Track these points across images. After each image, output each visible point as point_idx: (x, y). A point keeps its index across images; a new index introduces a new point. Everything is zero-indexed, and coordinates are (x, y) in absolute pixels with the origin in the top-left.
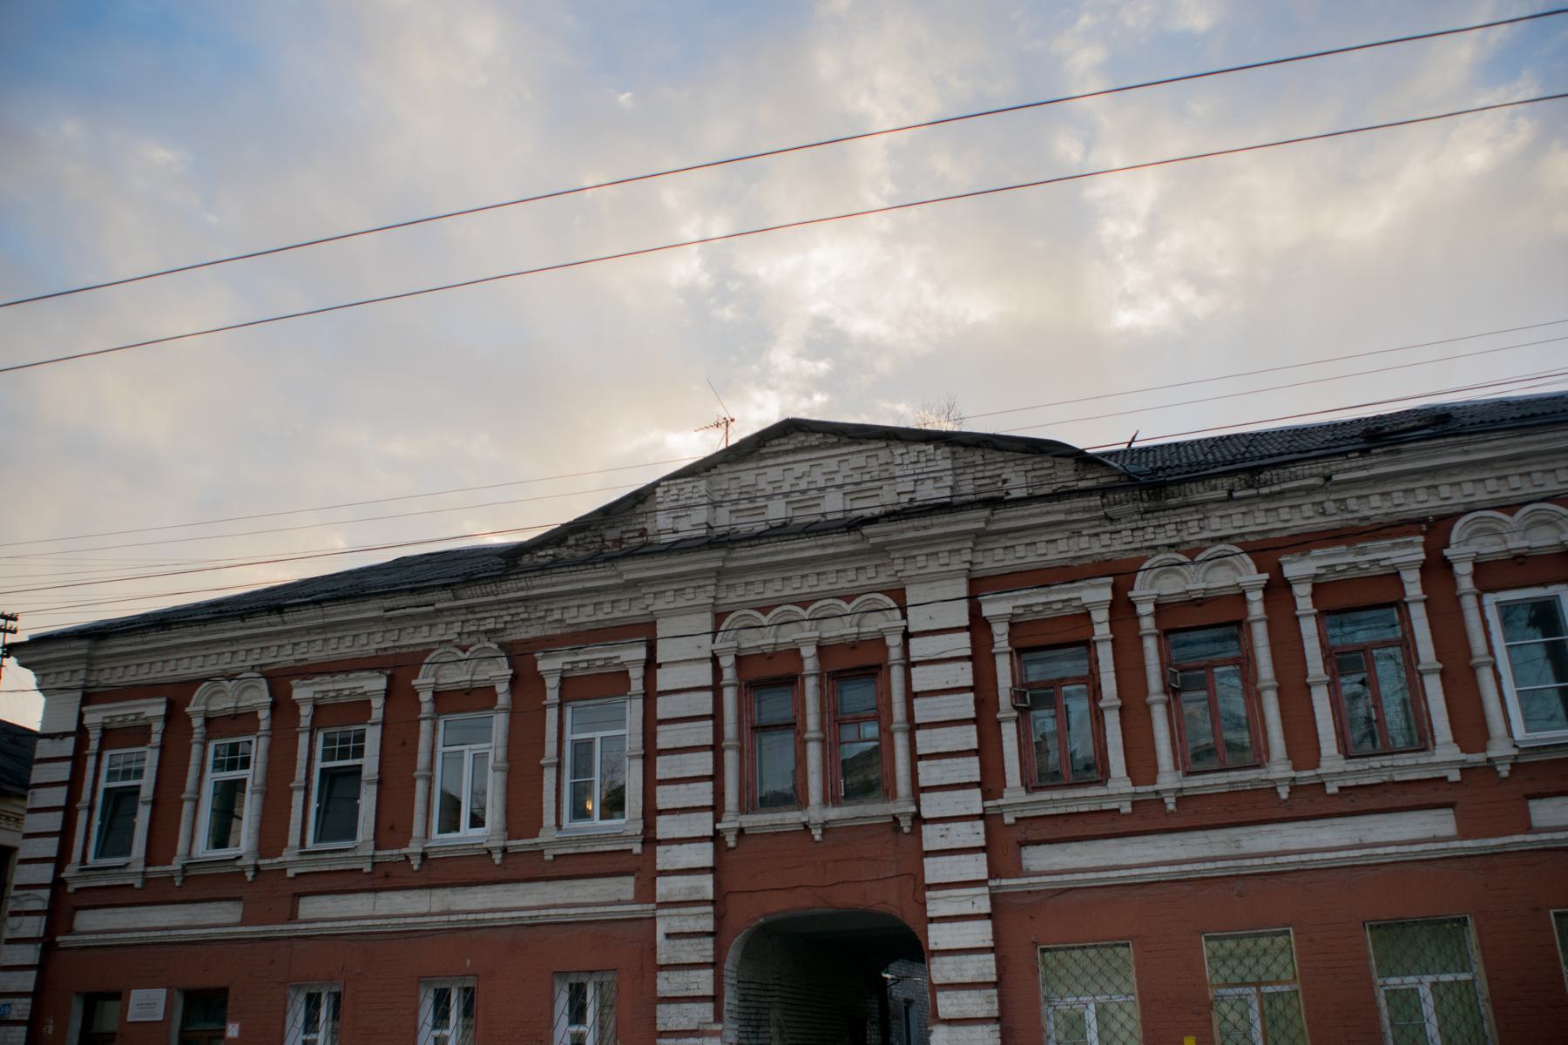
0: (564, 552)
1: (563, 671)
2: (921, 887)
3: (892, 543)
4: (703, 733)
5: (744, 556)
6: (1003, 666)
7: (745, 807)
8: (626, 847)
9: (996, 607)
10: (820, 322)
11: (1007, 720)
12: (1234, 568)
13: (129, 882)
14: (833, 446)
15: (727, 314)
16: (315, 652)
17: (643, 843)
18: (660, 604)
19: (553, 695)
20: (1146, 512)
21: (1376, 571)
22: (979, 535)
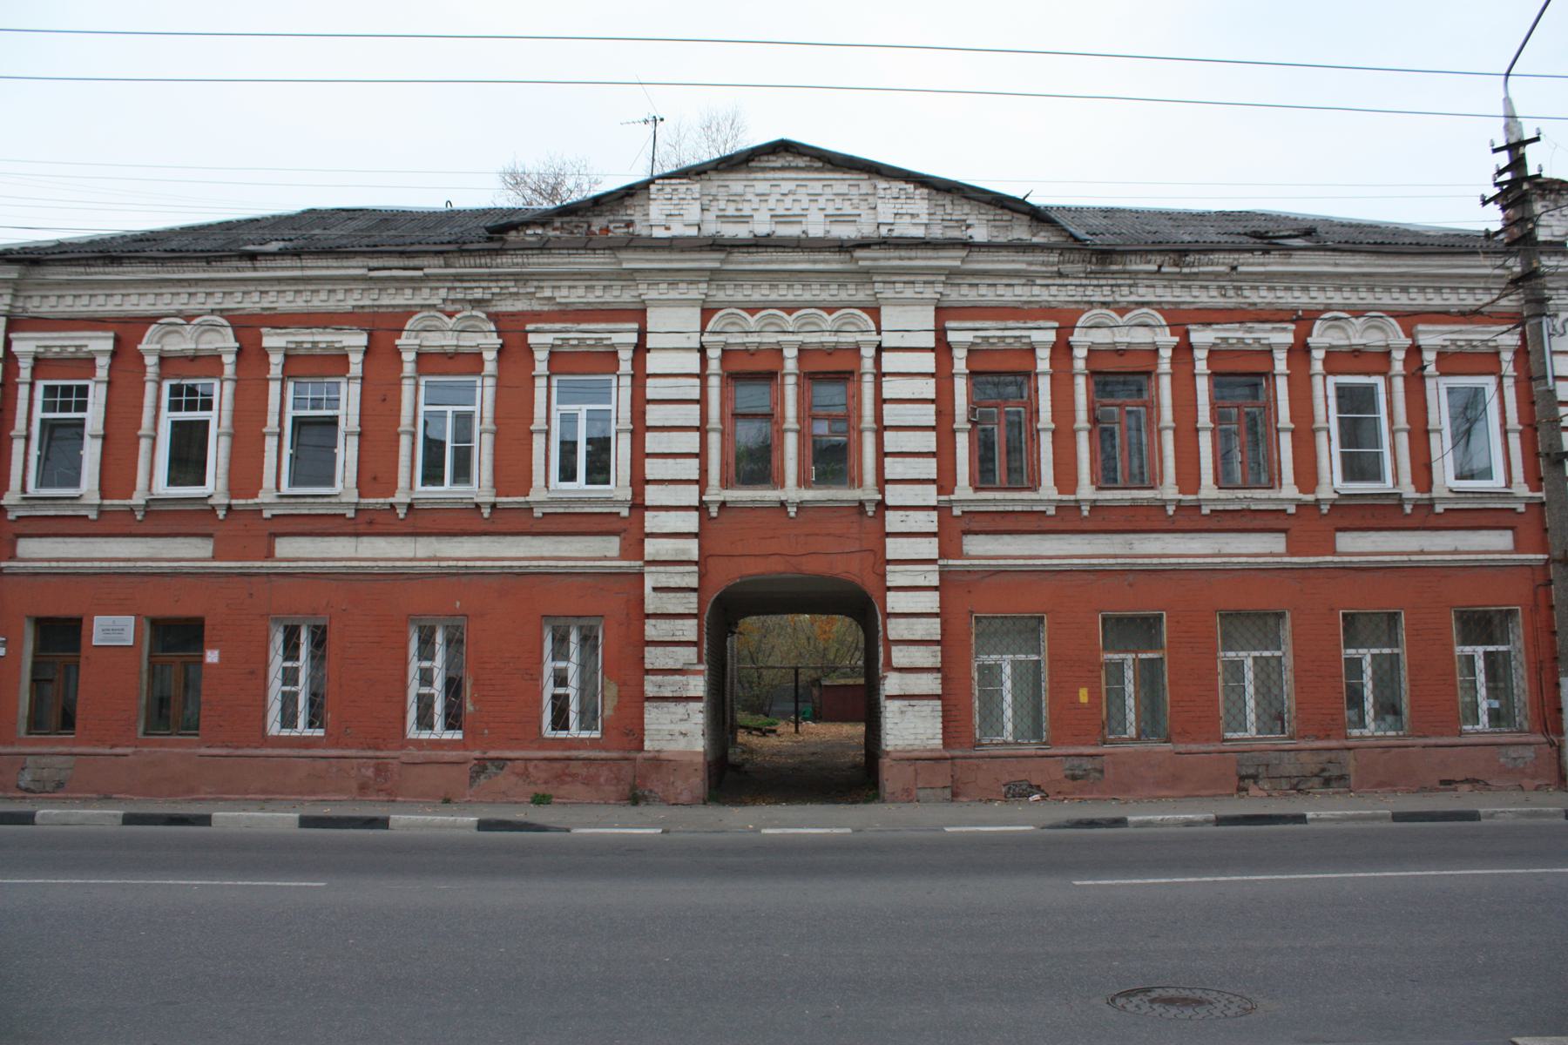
5: (741, 261)
6: (961, 386)
9: (960, 336)
11: (962, 430)
13: (83, 513)
14: (817, 170)
16: (287, 302)
18: (653, 294)
19: (276, 371)
21: (1257, 347)
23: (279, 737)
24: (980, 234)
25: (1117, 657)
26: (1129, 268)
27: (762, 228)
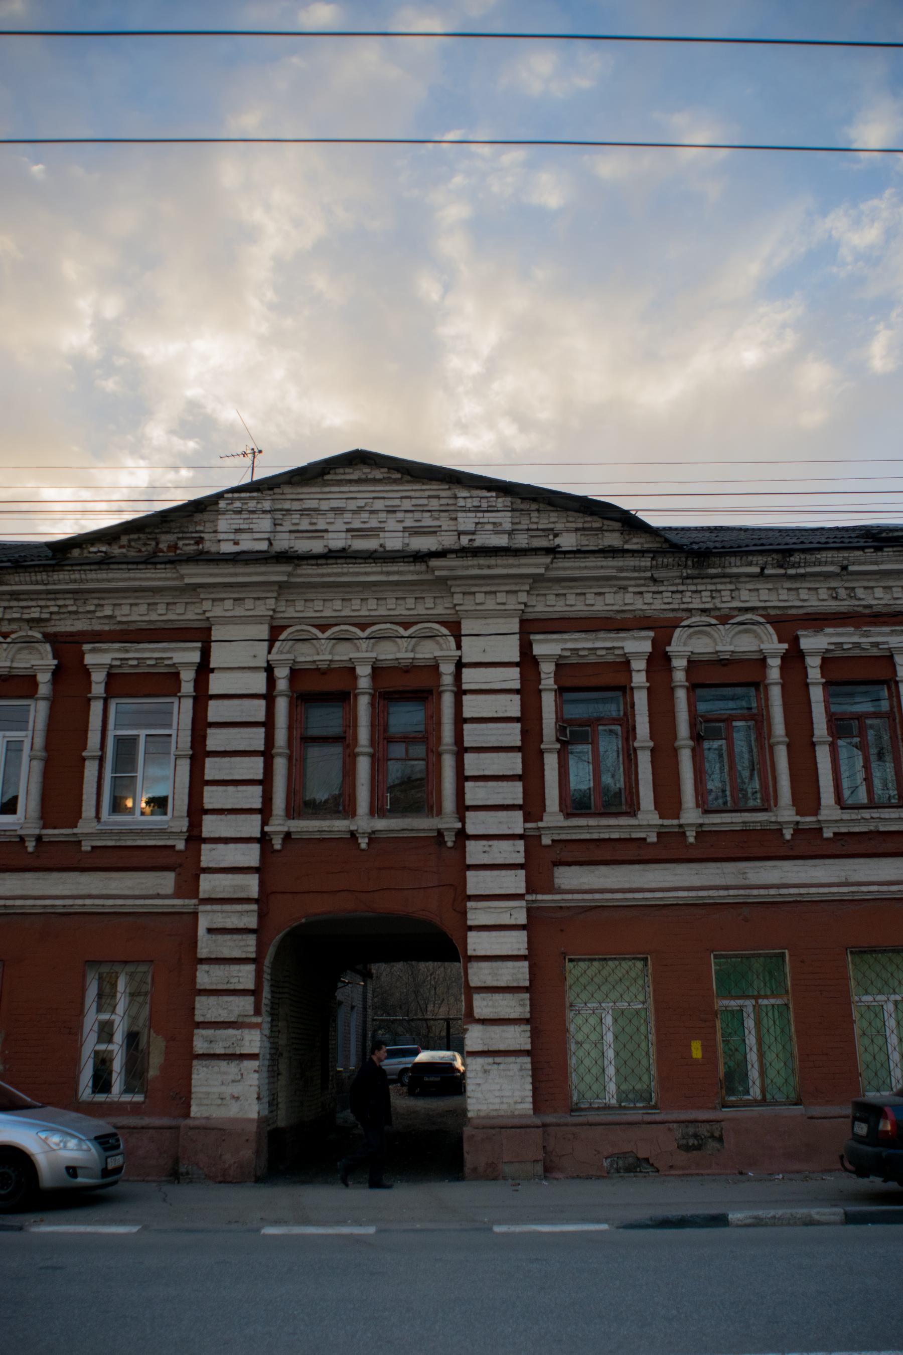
0: (116, 550)
1: (111, 666)
2: (462, 898)
3: (456, 578)
4: (255, 739)
5: (308, 573)
6: (548, 702)
7: (291, 812)
8: (169, 843)
9: (546, 647)
10: (193, 406)
11: (550, 751)
12: (757, 636)
14: (395, 481)
15: (110, 385)
17: (187, 841)
18: (217, 611)
19: (98, 689)
20: (687, 578)
21: (875, 652)
22: (536, 579)
23: (92, 1104)
24: (567, 541)
25: (734, 1004)
26: (728, 570)
27: (337, 542)
